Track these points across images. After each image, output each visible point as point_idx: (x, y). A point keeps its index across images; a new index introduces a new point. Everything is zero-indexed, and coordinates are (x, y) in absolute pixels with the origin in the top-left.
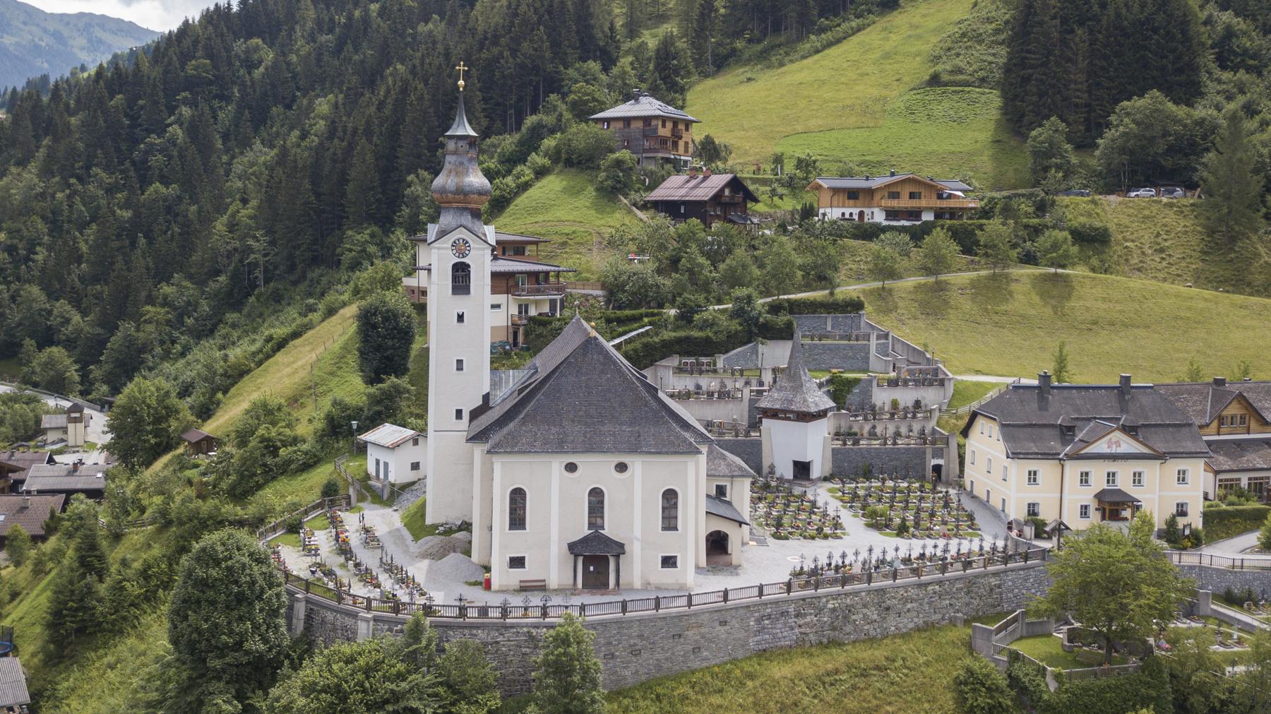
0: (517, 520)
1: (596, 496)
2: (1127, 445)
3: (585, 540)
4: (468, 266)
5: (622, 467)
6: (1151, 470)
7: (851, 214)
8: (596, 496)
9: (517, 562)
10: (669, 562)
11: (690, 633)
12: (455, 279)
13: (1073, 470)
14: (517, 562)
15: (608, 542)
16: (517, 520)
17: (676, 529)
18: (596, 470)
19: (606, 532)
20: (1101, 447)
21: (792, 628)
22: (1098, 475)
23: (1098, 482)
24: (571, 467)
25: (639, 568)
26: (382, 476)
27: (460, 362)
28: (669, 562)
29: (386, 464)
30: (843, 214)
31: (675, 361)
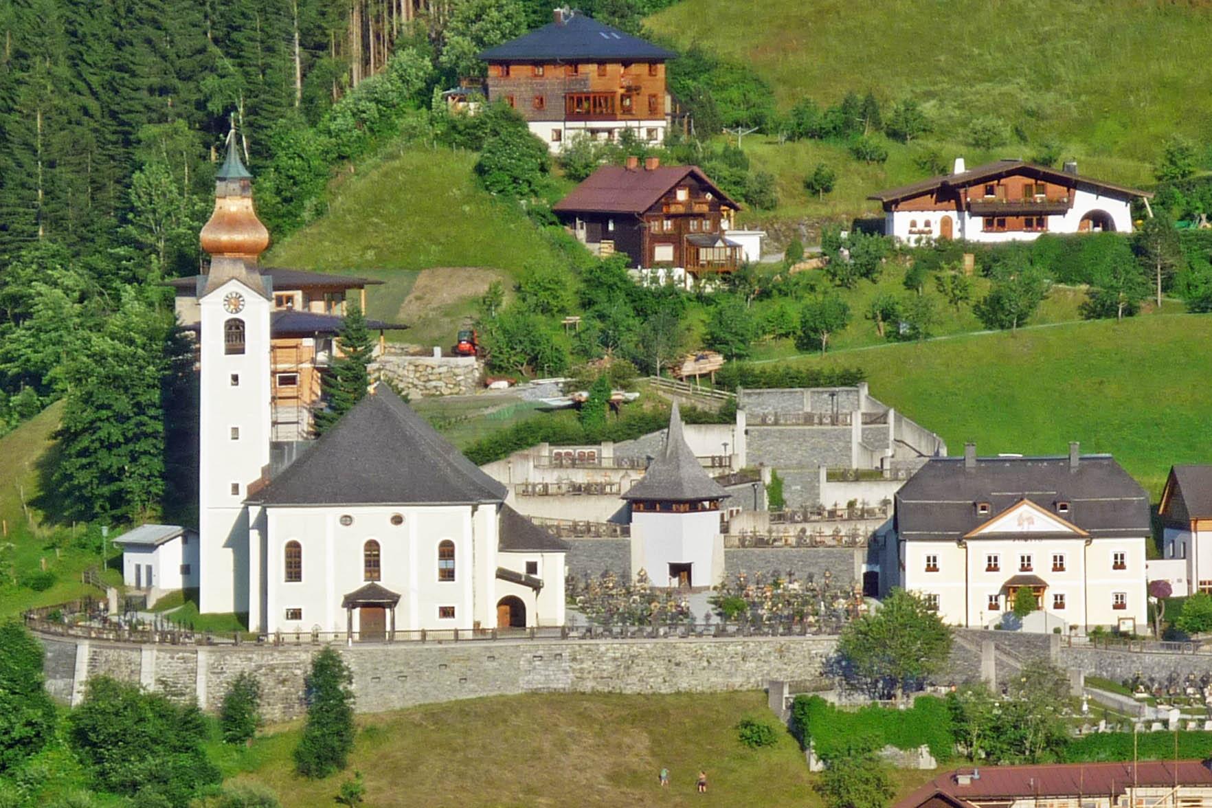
0: (294, 572)
1: (372, 549)
2: (1044, 521)
3: (361, 593)
4: (243, 322)
5: (398, 520)
6: (1072, 549)
7: (927, 224)
8: (372, 549)
9: (296, 614)
10: (447, 612)
11: (456, 665)
12: (229, 337)
13: (979, 550)
14: (296, 614)
15: (383, 593)
16: (294, 572)
17: (242, 351)
18: (372, 519)
19: (382, 583)
20: (1007, 522)
21: (566, 672)
22: (1010, 556)
23: (1010, 569)
24: (347, 520)
25: (413, 616)
26: (144, 584)
27: (235, 430)
28: (447, 612)
29: (149, 569)
30: (913, 224)
31: (546, 450)
